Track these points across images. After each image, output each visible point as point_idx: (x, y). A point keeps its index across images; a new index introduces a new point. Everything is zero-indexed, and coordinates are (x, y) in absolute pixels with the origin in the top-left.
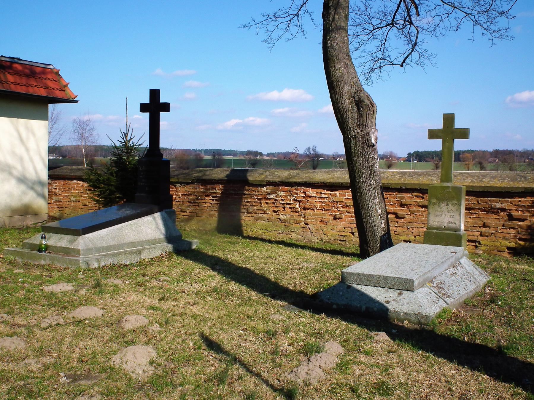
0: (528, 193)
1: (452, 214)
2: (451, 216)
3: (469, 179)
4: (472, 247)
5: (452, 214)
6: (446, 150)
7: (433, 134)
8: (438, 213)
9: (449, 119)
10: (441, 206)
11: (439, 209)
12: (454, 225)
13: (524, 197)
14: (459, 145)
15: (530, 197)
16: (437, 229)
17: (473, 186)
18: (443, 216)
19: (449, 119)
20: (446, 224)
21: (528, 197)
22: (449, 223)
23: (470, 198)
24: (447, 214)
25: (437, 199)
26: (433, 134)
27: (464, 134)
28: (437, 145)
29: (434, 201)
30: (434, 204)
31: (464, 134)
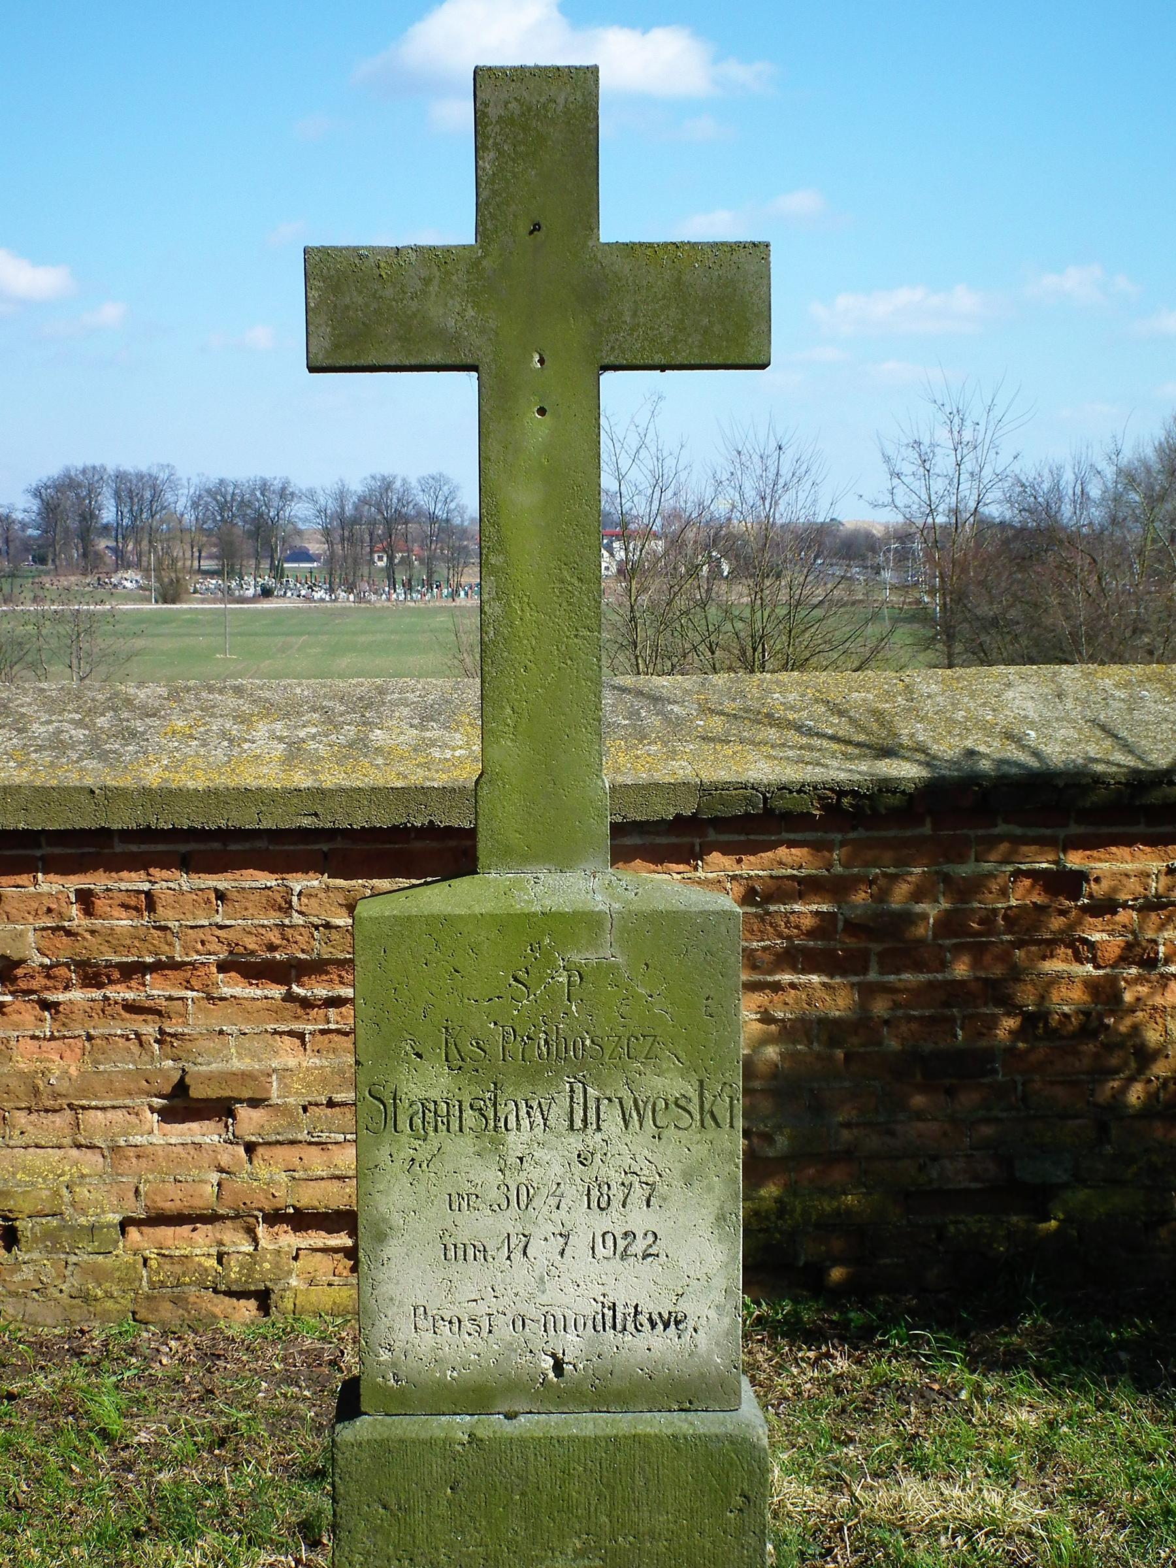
0: (720, 823)
1: (639, 1219)
2: (623, 1246)
3: (262, 730)
4: (323, 1264)
5: (639, 1219)
6: (524, 497)
7: (362, 315)
8: (477, 1225)
9: (537, 130)
10: (516, 1142)
11: (488, 1176)
12: (659, 1345)
13: (689, 855)
14: (667, 438)
15: (726, 850)
16: (476, 1397)
17: (320, 793)
18: (543, 1250)
19: (537, 130)
20: (572, 1344)
21: (715, 857)
22: (610, 1318)
23: (298, 882)
24: (588, 1224)
25: (457, 1061)
26: (362, 315)
27: (711, 311)
28: (418, 433)
29: (427, 1082)
30: (432, 1118)
31: (711, 311)
